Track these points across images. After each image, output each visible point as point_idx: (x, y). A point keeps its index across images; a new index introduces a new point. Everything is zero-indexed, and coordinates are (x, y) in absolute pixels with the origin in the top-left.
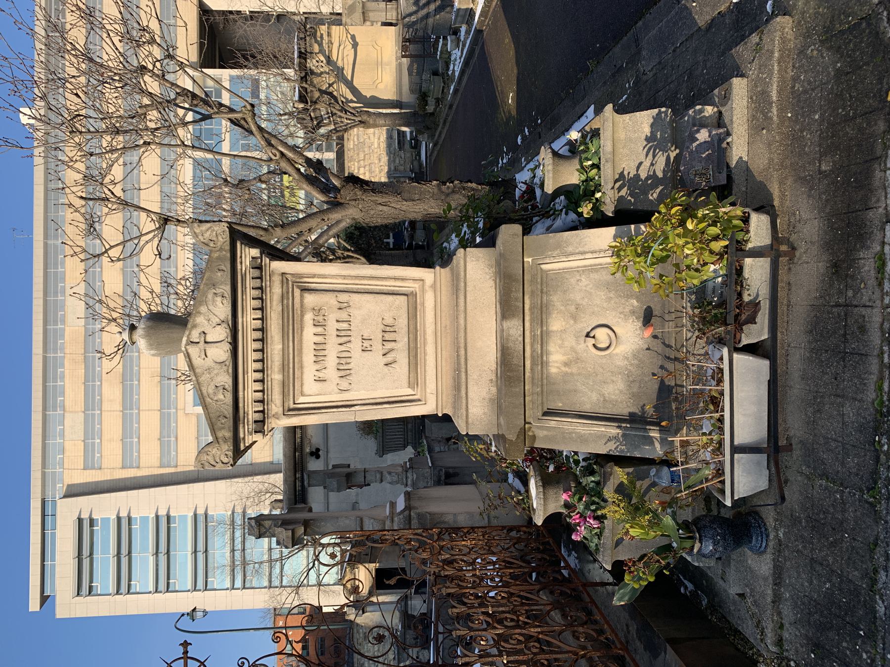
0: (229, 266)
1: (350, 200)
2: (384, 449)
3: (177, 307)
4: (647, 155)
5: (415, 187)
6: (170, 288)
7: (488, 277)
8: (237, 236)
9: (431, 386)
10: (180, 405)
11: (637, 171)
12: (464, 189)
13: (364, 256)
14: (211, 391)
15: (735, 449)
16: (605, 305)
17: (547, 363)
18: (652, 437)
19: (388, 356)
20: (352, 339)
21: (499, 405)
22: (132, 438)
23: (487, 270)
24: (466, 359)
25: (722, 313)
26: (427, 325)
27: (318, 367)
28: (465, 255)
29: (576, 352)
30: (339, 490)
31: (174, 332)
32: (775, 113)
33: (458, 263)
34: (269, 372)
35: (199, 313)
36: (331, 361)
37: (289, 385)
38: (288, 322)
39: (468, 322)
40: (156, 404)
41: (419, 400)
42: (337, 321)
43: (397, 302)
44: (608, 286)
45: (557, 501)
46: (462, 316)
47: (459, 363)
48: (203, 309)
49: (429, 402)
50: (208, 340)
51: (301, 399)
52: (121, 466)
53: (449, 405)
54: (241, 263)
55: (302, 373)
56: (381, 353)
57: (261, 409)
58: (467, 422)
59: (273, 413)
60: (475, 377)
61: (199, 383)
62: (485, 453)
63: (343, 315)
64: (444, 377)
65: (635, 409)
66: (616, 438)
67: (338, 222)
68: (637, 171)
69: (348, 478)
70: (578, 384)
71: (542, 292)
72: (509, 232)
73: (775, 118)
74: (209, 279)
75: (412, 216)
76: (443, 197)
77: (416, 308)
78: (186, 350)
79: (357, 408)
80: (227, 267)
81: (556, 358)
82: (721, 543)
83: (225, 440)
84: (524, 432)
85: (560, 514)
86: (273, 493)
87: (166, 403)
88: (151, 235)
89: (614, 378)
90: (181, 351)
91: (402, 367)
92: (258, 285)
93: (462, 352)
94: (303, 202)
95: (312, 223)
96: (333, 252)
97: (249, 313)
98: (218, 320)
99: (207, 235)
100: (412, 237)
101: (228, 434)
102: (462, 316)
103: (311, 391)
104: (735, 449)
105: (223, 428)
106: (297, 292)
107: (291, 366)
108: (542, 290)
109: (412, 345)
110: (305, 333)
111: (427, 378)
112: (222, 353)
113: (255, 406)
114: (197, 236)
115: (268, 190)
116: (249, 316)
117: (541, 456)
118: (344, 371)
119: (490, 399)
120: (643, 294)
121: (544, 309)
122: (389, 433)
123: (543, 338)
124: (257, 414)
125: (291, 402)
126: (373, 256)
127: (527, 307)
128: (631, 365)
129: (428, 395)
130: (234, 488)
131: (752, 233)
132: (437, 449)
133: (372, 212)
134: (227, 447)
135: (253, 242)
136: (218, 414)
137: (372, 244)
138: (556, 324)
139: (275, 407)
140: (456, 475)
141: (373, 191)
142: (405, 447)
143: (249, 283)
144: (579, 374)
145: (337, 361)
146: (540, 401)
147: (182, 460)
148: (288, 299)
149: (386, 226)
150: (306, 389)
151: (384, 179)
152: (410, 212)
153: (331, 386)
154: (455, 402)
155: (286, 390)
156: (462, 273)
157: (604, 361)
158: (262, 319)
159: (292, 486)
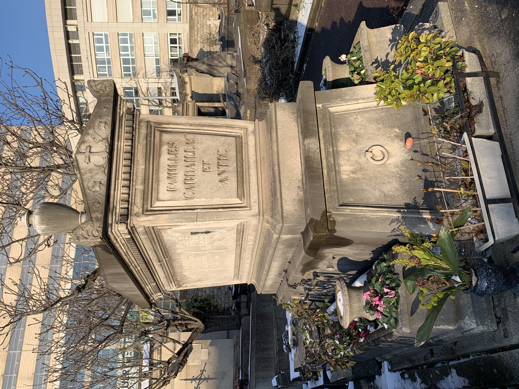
0: (112, 105)
4: (391, 50)
7: (292, 120)
9: (254, 197)
11: (387, 58)
14: (90, 185)
15: (487, 202)
16: (376, 133)
17: (339, 172)
18: (425, 218)
25: (457, 117)
29: (359, 164)
32: (467, 5)
33: (270, 115)
35: (88, 134)
36: (180, 177)
39: (280, 149)
43: (228, 141)
44: (377, 121)
45: (360, 301)
48: (91, 131)
49: (253, 208)
54: (120, 109)
55: (158, 185)
56: (217, 173)
57: (126, 206)
58: (282, 217)
61: (82, 180)
63: (190, 148)
64: (264, 192)
65: (410, 201)
66: (397, 220)
68: (387, 58)
70: (364, 185)
73: (468, 8)
77: (242, 146)
78: (76, 157)
81: (346, 169)
82: (493, 275)
83: (97, 219)
85: (349, 78)
89: (390, 180)
91: (232, 183)
93: (276, 168)
97: (122, 141)
101: (100, 215)
104: (487, 202)
105: (97, 211)
106: (157, 134)
107: (150, 181)
108: (331, 124)
109: (239, 170)
110: (161, 158)
111: (251, 191)
112: (101, 159)
113: (122, 204)
118: (189, 183)
119: (299, 200)
120: (402, 125)
121: (335, 154)
123: (336, 154)
124: (123, 210)
125: (149, 206)
126: (207, 320)
128: (401, 170)
129: (252, 203)
131: (467, 63)
134: (98, 225)
138: (343, 146)
139: (137, 209)
144: (364, 179)
146: (336, 196)
148: (151, 137)
150: (161, 196)
155: (146, 197)
157: (381, 169)
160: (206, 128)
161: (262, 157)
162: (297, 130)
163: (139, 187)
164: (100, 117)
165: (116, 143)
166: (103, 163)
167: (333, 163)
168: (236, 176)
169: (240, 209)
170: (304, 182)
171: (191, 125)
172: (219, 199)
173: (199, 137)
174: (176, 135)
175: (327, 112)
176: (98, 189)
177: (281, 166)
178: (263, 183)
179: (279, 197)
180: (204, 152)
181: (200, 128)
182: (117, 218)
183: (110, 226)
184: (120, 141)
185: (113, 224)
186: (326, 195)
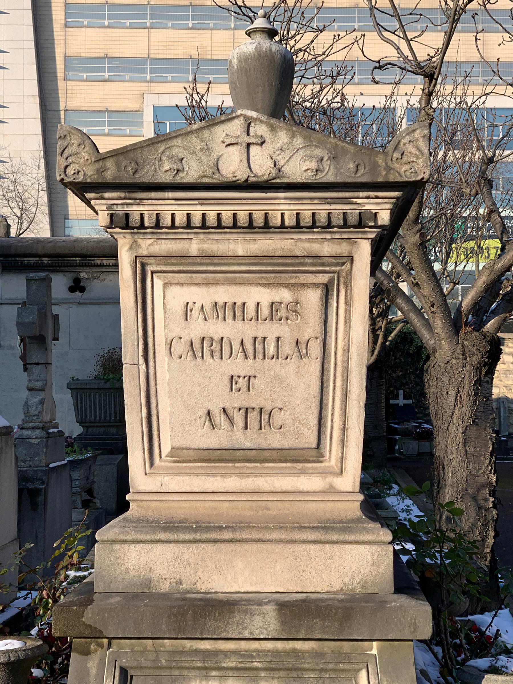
1: (463, 346)
2: (78, 390)
3: (303, 90)
5: (486, 445)
6: (329, 80)
7: (347, 580)
8: (409, 193)
9: (173, 483)
10: (155, 87)
12: (485, 525)
13: (376, 361)
14: (175, 151)
19: (223, 416)
20: (250, 361)
21: (140, 595)
22: (109, 125)
23: (358, 579)
24: (215, 541)
26: (269, 479)
27: (208, 308)
28: (383, 543)
30: (18, 324)
31: (264, 96)
34: (202, 236)
35: (293, 136)
36: (217, 329)
37: (180, 264)
38: (278, 265)
40: (157, 53)
41: (152, 464)
42: (278, 339)
43: (306, 432)
46: (284, 536)
47: (208, 529)
48: (299, 142)
50: (253, 149)
51: (158, 283)
52: (67, 55)
53: (143, 512)
54: (368, 198)
55: (198, 284)
56: (228, 406)
57: (146, 224)
58: (114, 542)
59: (140, 241)
60: (186, 557)
61: (187, 134)
62: (65, 562)
63: (287, 348)
67: (428, 325)
69: (37, 338)
71: (322, 670)
72: (418, 616)
74: (345, 152)
75: (439, 439)
76: (470, 491)
77: (297, 461)
78: (237, 117)
79: (143, 367)
80: (363, 177)
83: (100, 171)
84: (96, 635)
86: (20, 219)
87: (159, 67)
88: (407, 52)
90: (238, 104)
92: (334, 222)
93: (226, 535)
94: (460, 268)
95: (427, 289)
96: (384, 314)
97: (292, 207)
98: (282, 163)
99: (411, 148)
100: (406, 434)
101: (109, 176)
102: (284, 536)
103: (170, 298)
106: (323, 279)
108: (326, 671)
109: (238, 454)
110: (260, 289)
111: (187, 478)
112: (232, 169)
113: (150, 215)
114: (408, 134)
115: (477, 218)
116: (287, 207)
117: (56, 655)
118: (201, 348)
122: (102, 397)
124: (138, 218)
127: (298, 645)
129: (160, 478)
130: (29, 162)
132: (76, 475)
133: (445, 379)
134: (89, 174)
135: (399, 214)
136: (141, 161)
137: (397, 370)
139: (148, 245)
140: (34, 506)
141: (479, 382)
142: (81, 422)
143: (337, 208)
145: (217, 338)
146: (144, 663)
147: (75, 87)
148: (313, 265)
149: (423, 394)
150: (174, 291)
151: (496, 392)
152: (446, 438)
153: (178, 327)
154: (147, 521)
155: (173, 260)
156: (352, 538)
158: (283, 226)
159: (29, 252)
160: (339, 383)
161: (270, 504)
162: (319, 589)
163: (194, 246)
164: (334, 158)
165: (281, 195)
166: (313, 168)
167: (224, 665)
168: (222, 447)
169: (146, 453)
170: (188, 596)
171: (347, 351)
172: (169, 409)
173: (315, 367)
174: (317, 318)
175: (356, 667)
176: (166, 166)
177: (232, 546)
178: (208, 505)
179: (157, 538)
180: (278, 379)
181: (339, 370)
182: (120, 208)
183: (97, 195)
184: (289, 201)
185: (104, 202)
186: (150, 642)
